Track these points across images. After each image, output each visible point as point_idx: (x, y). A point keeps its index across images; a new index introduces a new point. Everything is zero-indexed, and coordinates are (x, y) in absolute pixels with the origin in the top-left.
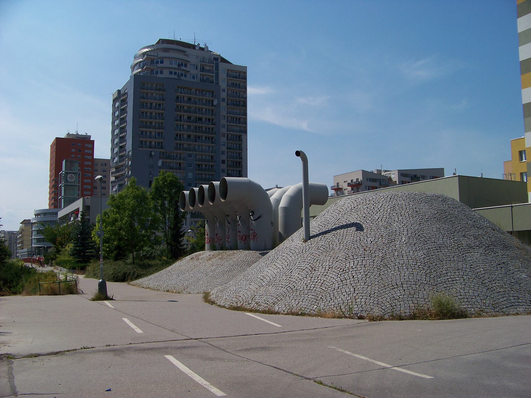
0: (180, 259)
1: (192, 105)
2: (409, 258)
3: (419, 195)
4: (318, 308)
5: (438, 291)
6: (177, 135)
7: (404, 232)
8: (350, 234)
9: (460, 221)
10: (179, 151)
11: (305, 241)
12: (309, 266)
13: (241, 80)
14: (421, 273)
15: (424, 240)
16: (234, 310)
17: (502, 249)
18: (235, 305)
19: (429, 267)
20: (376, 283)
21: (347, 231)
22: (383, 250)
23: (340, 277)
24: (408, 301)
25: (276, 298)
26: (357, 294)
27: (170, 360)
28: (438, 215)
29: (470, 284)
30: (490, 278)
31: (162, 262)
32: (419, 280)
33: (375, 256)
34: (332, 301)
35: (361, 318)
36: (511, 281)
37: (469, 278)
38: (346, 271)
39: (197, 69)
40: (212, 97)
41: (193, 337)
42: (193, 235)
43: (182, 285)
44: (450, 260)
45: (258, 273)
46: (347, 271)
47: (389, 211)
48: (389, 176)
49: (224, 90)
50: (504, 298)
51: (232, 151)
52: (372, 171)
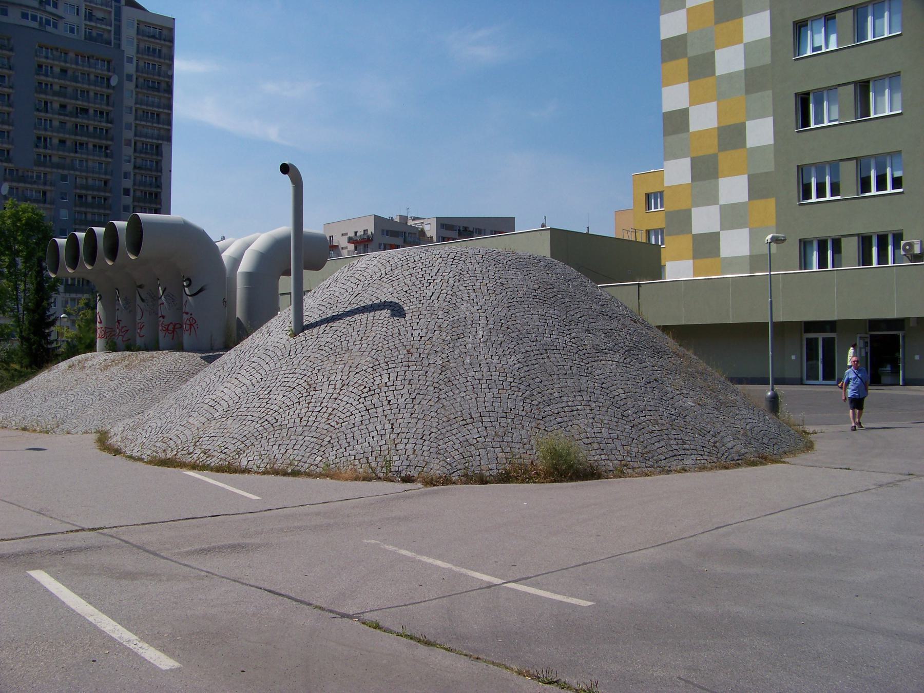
0: (47, 368)
1: (68, 83)
2: (491, 368)
3: (506, 255)
4: (324, 460)
5: (546, 429)
6: (39, 138)
7: (480, 320)
8: (380, 322)
9: (578, 303)
10: (42, 169)
11: (295, 334)
12: (302, 381)
13: (163, 42)
14: (514, 397)
15: (517, 335)
16: (160, 465)
17: (651, 356)
18: (162, 455)
19: (529, 385)
20: (433, 414)
21: (374, 317)
22: (443, 353)
23: (363, 403)
24: (493, 447)
25: (243, 442)
26: (398, 434)
27: (42, 582)
28: (540, 292)
29: (603, 416)
30: (636, 406)
31: (10, 374)
32: (511, 410)
33: (429, 364)
34: (351, 448)
35: (407, 480)
36: (671, 413)
37: (600, 407)
38: (374, 390)
39: (78, 14)
40: (109, 70)
41: (86, 527)
42: (69, 324)
43: (52, 416)
44: (566, 374)
45: (204, 394)
46: (376, 391)
47: (451, 281)
48: (421, 227)
49: (130, 60)
50: (661, 443)
51: (143, 172)
52: (392, 218)
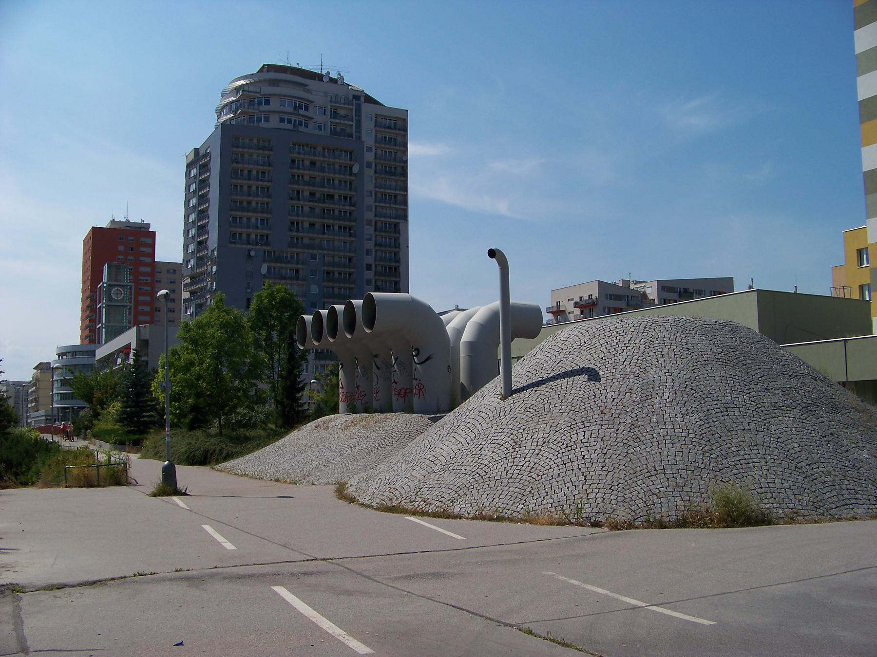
0: (297, 428)
1: (317, 173)
2: (675, 425)
3: (693, 322)
4: (525, 508)
5: (723, 480)
6: (292, 223)
7: (667, 383)
8: (578, 386)
9: (759, 364)
10: (295, 250)
11: (504, 398)
12: (510, 439)
13: (398, 132)
14: (695, 451)
15: (700, 396)
16: (386, 512)
17: (829, 412)
18: (388, 503)
19: (709, 441)
20: (622, 467)
21: (573, 381)
22: (632, 413)
23: (561, 458)
24: (673, 496)
25: (456, 492)
26: (590, 485)
27: (281, 594)
28: (723, 356)
29: (777, 468)
30: (810, 458)
31: (267, 433)
32: (692, 462)
33: (620, 422)
34: (549, 497)
35: (596, 524)
36: (845, 464)
37: (775, 460)
38: (571, 447)
39: (325, 114)
40: (351, 159)
41: (319, 557)
42: (319, 388)
43: (300, 470)
44: (743, 430)
45: (426, 451)
46: (572, 447)
47: (642, 348)
48: (643, 290)
49: (369, 149)
50: (832, 492)
51: (383, 248)
52: (615, 283)
